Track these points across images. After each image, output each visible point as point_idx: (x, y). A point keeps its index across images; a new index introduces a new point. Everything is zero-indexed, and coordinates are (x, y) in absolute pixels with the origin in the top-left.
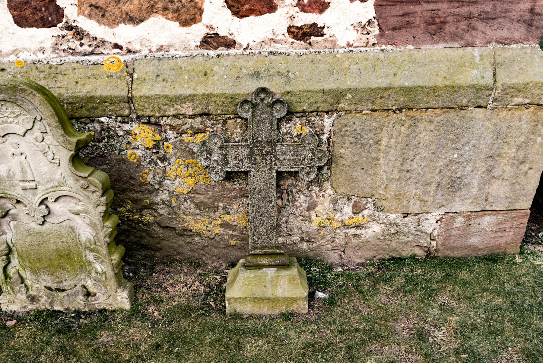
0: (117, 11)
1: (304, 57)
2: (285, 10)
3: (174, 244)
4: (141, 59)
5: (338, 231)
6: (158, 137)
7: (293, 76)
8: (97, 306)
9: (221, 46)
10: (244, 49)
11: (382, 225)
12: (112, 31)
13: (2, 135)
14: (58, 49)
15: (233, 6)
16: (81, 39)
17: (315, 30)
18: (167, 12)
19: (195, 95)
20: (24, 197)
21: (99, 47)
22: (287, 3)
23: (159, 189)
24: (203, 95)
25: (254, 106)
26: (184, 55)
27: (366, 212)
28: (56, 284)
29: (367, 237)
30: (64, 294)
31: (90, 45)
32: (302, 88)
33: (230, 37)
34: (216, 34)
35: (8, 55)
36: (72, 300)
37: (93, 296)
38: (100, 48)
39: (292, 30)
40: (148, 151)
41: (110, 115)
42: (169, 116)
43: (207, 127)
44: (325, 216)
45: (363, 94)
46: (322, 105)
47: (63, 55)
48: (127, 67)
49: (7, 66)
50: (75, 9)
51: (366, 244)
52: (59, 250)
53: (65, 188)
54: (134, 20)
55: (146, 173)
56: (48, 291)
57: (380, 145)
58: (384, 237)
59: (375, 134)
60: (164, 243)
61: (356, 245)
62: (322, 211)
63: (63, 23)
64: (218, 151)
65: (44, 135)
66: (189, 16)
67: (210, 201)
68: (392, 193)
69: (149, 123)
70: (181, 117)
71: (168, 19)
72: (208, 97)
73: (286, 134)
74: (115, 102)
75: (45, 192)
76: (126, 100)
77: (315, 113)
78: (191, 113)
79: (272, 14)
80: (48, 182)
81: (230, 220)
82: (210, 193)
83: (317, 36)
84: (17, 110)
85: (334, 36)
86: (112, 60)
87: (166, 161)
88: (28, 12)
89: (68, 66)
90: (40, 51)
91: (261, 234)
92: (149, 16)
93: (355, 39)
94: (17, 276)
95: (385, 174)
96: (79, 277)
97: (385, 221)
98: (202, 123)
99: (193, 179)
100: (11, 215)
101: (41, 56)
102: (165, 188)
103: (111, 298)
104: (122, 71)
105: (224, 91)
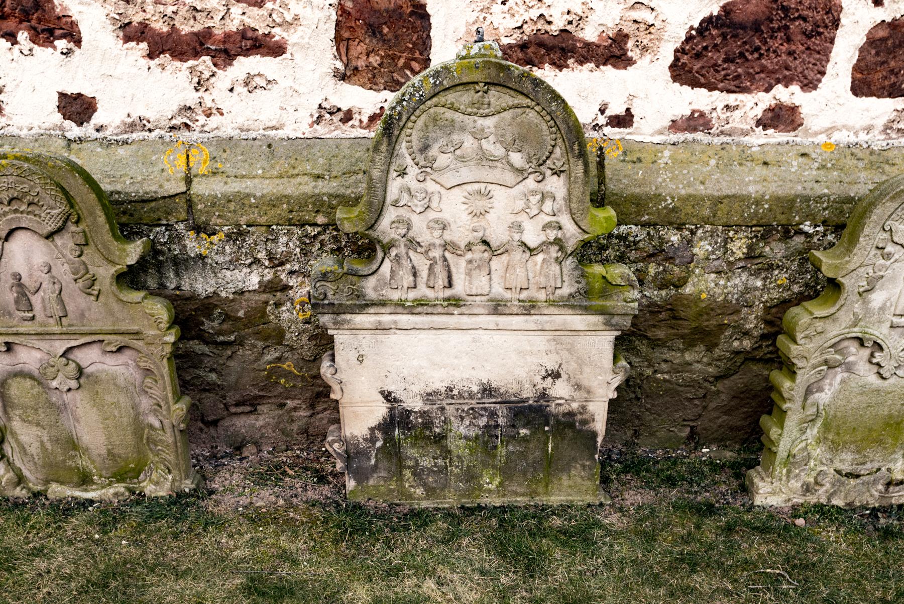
8: (893, 501)
13: (3, 234)
14: (891, 128)
30: (858, 481)
35: (816, 134)
49: (811, 150)
56: (837, 476)
89: (896, 152)
96: (893, 456)
101: (863, 137)
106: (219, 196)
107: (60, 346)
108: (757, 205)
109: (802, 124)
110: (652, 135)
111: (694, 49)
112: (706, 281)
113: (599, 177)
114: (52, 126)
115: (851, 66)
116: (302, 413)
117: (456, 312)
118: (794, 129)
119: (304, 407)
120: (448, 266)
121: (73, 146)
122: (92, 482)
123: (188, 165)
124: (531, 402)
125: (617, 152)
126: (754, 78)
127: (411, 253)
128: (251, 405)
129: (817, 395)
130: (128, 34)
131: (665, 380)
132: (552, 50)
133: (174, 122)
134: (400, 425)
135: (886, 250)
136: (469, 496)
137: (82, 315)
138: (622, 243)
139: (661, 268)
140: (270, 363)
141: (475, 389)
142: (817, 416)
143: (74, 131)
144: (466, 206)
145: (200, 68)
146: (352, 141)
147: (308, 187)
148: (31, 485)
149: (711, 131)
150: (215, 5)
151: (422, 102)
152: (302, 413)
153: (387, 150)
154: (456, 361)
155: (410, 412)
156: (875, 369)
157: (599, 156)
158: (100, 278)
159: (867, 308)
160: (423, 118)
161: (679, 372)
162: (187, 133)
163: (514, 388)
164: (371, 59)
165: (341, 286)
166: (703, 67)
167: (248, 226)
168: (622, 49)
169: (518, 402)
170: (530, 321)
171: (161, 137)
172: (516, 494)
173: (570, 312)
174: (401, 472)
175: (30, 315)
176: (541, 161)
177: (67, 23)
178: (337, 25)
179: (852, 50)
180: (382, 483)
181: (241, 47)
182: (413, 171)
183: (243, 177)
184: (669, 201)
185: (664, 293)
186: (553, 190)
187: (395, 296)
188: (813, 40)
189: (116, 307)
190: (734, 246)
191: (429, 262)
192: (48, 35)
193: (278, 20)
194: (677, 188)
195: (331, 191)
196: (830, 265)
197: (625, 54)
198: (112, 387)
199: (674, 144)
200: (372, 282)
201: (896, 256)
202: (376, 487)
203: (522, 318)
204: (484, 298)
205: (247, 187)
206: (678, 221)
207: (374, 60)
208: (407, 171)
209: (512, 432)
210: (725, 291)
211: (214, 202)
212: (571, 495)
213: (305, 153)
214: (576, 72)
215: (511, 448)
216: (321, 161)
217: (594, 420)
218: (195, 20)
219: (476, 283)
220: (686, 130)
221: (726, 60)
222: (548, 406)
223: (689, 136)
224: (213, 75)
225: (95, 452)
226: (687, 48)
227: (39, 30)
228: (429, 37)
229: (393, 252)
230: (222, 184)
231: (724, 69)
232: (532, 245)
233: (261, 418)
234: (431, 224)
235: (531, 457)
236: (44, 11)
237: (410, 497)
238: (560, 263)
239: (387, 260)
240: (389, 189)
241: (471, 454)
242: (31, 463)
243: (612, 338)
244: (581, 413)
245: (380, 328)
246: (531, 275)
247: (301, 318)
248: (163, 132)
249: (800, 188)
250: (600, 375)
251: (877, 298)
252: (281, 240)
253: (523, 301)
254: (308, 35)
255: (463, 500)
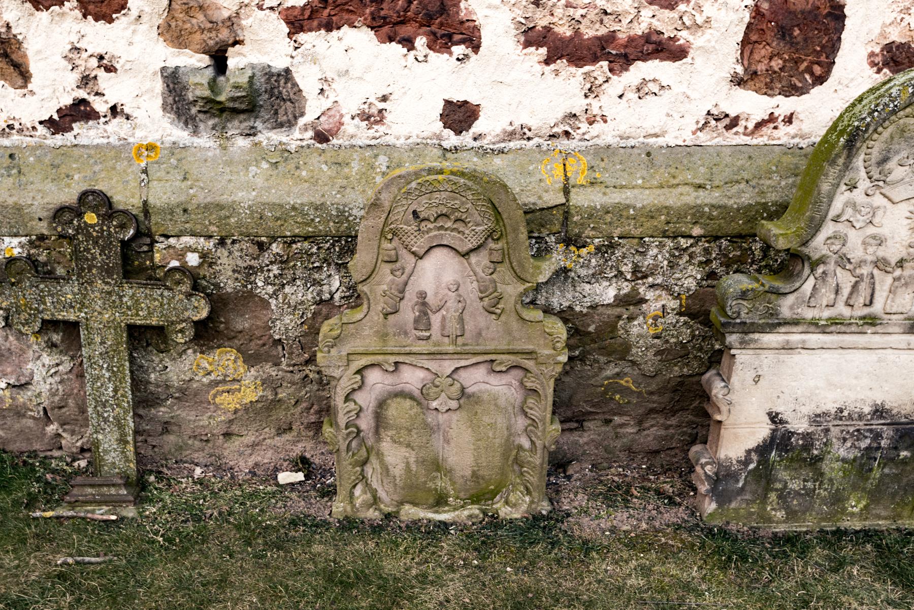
106: (598, 207)
107: (448, 366)
114: (430, 134)
116: (630, 430)
117: (869, 331)
119: (632, 423)
120: (874, 284)
121: (449, 155)
122: (446, 503)
123: (566, 176)
127: (839, 270)
128: (577, 421)
130: (529, 39)
133: (555, 130)
134: (783, 444)
136: (829, 520)
137: (479, 334)
140: (608, 378)
141: (867, 410)
143: (451, 139)
144: (910, 221)
145: (595, 74)
146: (733, 149)
147: (691, 197)
148: (382, 506)
150: (627, 8)
151: (894, 112)
152: (630, 430)
153: (844, 164)
154: (854, 382)
155: (793, 433)
158: (506, 296)
160: (891, 129)
162: (566, 142)
164: (773, 63)
165: (757, 305)
167: (619, 238)
169: (908, 424)
171: (539, 146)
172: (879, 517)
174: (766, 494)
175: (428, 334)
177: (469, 27)
178: (748, 27)
180: (744, 506)
181: (642, 52)
182: (864, 184)
183: (622, 187)
187: (809, 314)
189: (515, 324)
191: (854, 280)
192: (447, 40)
193: (688, 23)
195: (714, 202)
198: (492, 407)
200: (791, 299)
202: (736, 510)
204: (902, 316)
205: (627, 198)
207: (776, 64)
208: (858, 185)
209: (893, 453)
211: (592, 214)
213: (685, 162)
215: (886, 471)
216: (702, 170)
218: (601, 23)
219: (899, 300)
224: (607, 81)
225: (458, 473)
227: (439, 35)
228: (839, 39)
229: (820, 270)
230: (600, 195)
233: (586, 434)
234: (868, 240)
235: (905, 480)
236: (449, 15)
237: (770, 520)
239: (812, 278)
240: (834, 203)
241: (843, 478)
242: (391, 485)
245: (788, 348)
247: (652, 332)
248: (541, 141)
252: (651, 253)
254: (716, 39)
255: (823, 524)
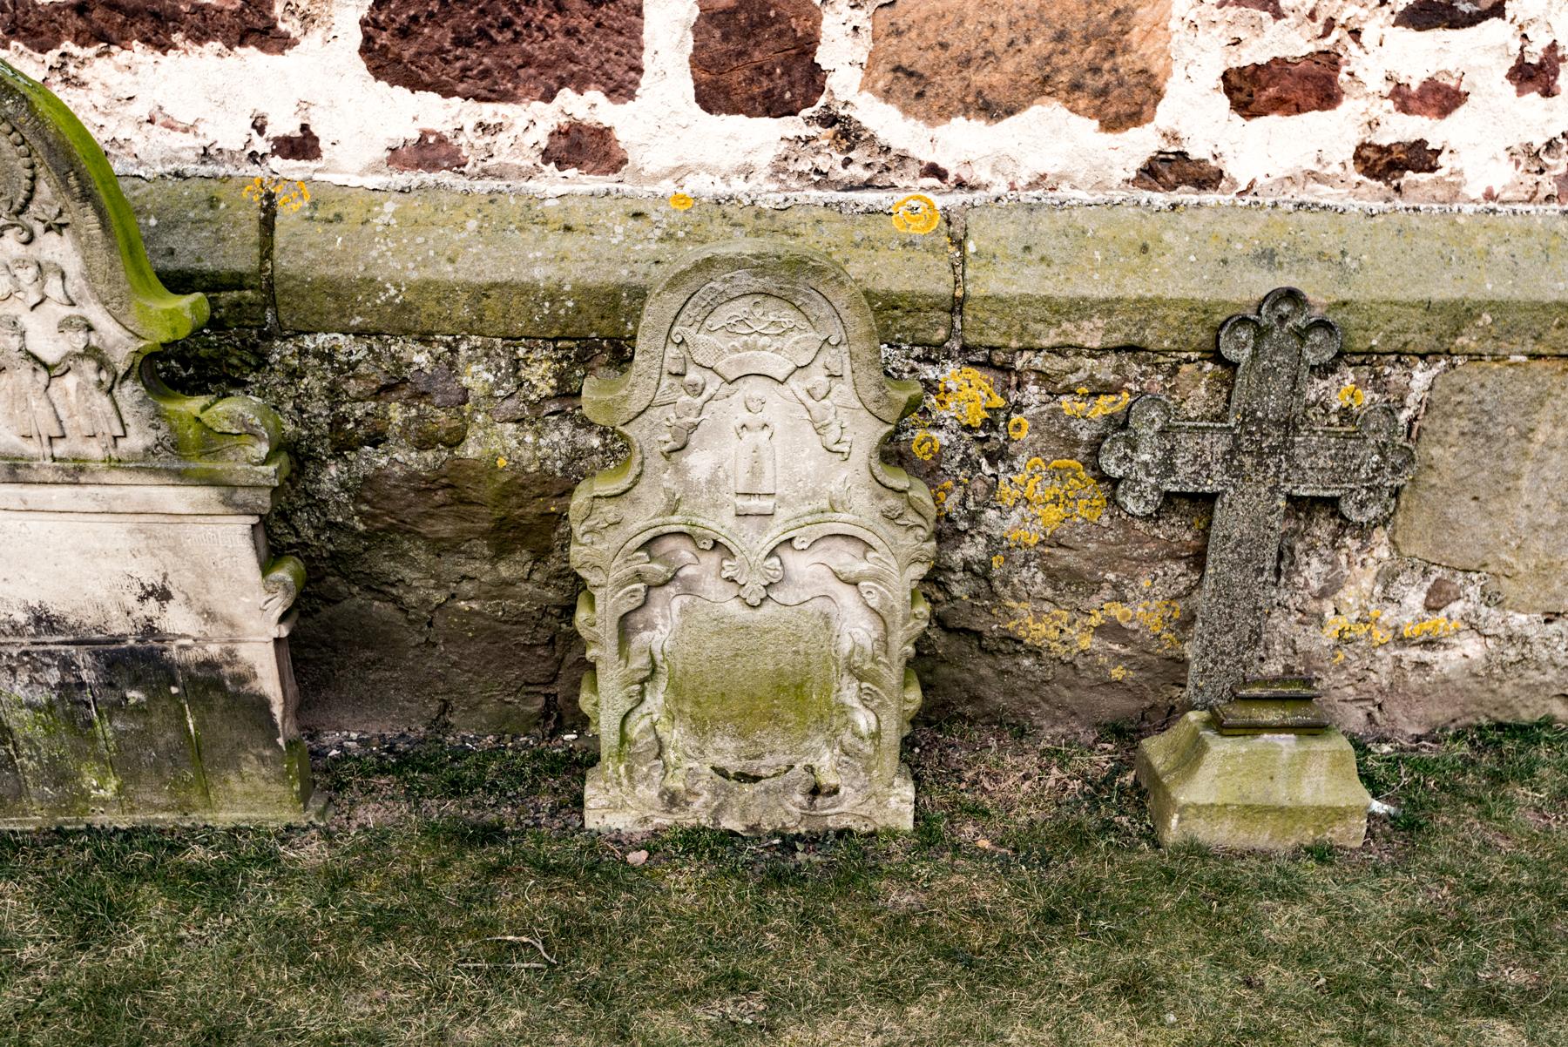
0: (955, 86)
1: (1380, 220)
2: (1362, 104)
3: (967, 676)
4: (986, 205)
5: (1380, 652)
6: (999, 401)
7: (1355, 265)
8: (830, 823)
9: (1185, 182)
10: (1239, 194)
11: (1489, 641)
12: (931, 132)
14: (785, 171)
15: (1240, 90)
16: (850, 149)
17: (1420, 157)
18: (1077, 94)
19: (1118, 300)
20: (734, 535)
21: (888, 169)
22: (1369, 89)
23: (966, 532)
24: (1140, 300)
25: (1261, 333)
26: (1091, 200)
27: (1456, 608)
28: (744, 761)
29: (1446, 671)
30: (757, 787)
31: (868, 166)
32: (1377, 293)
33: (1213, 163)
34: (1182, 155)
35: (656, 178)
36: (772, 803)
37: (829, 794)
38: (892, 173)
39: (1366, 153)
40: (966, 435)
41: (899, 340)
42: (1040, 350)
43: (1127, 380)
44: (1356, 615)
45: (1520, 316)
46: (1418, 338)
47: (795, 185)
48: (949, 223)
50: (857, 75)
51: (1440, 687)
52: (780, 673)
53: (845, 516)
54: (990, 109)
55: (944, 490)
56: (718, 779)
57: (1530, 441)
58: (1486, 674)
59: (1525, 414)
60: (944, 670)
61: (1415, 688)
62: (1351, 601)
63: (817, 107)
64: (1155, 440)
65: (834, 381)
66: (1123, 100)
67: (1087, 567)
68: (1532, 562)
69: (988, 364)
70: (1070, 353)
71: (1076, 112)
72: (1148, 307)
73: (1314, 404)
74: (919, 310)
75: (793, 524)
76: (948, 304)
77: (1393, 358)
78: (1096, 344)
79: (1328, 113)
80: (803, 499)
81: (1125, 616)
82: (1092, 546)
83: (1418, 170)
84: (788, 316)
85: (1460, 173)
86: (915, 204)
87: (1004, 461)
88: (737, 77)
89: (802, 213)
90: (739, 172)
91: (1222, 653)
92: (1031, 102)
93: (1507, 181)
94: (652, 738)
95: (1525, 514)
96: (807, 744)
97: (1501, 631)
98: (1118, 370)
99: (1061, 509)
100: (686, 578)
101: (738, 186)
102: (983, 528)
103: (873, 801)
104: (936, 232)
105: (1191, 294)
108: (552, 302)
109: (624, 161)
110: (361, 174)
111: (393, 21)
112: (501, 436)
113: (262, 247)
115: (686, 58)
118: (615, 170)
124: (131, 642)
125: (300, 203)
126: (517, 76)
129: (645, 635)
131: (471, 612)
132: (135, 15)
135: (687, 378)
138: (326, 365)
139: (414, 412)
142: (654, 671)
149: (465, 170)
156: (734, 590)
157: (265, 210)
159: (685, 481)
161: (493, 598)
163: (91, 618)
166: (419, 54)
168: (264, 16)
169: (107, 643)
170: (81, 497)
172: (156, 808)
173: (152, 479)
176: (16, 207)
179: (679, 31)
184: (393, 292)
185: (429, 455)
186: (57, 259)
188: (603, 8)
190: (532, 373)
194: (405, 268)
196: (595, 403)
197: (274, 27)
199: (402, 191)
201: (710, 390)
203: (67, 490)
206: (418, 328)
209: (113, 696)
210: (539, 454)
212: (254, 810)
214: (194, 57)
217: (255, 676)
220: (418, 166)
221: (457, 42)
222: (165, 650)
223: (429, 178)
226: (382, 17)
231: (457, 58)
232: (50, 357)
238: (110, 391)
241: (49, 735)
243: (246, 529)
244: (228, 663)
246: (63, 414)
249: (625, 272)
250: (242, 594)
251: (699, 463)
253: (61, 460)
255: (60, 818)
